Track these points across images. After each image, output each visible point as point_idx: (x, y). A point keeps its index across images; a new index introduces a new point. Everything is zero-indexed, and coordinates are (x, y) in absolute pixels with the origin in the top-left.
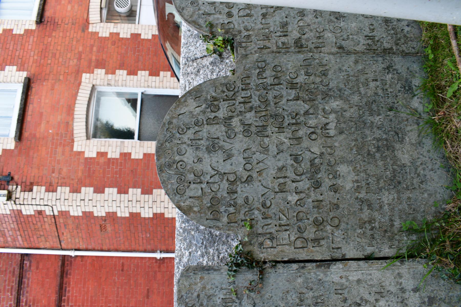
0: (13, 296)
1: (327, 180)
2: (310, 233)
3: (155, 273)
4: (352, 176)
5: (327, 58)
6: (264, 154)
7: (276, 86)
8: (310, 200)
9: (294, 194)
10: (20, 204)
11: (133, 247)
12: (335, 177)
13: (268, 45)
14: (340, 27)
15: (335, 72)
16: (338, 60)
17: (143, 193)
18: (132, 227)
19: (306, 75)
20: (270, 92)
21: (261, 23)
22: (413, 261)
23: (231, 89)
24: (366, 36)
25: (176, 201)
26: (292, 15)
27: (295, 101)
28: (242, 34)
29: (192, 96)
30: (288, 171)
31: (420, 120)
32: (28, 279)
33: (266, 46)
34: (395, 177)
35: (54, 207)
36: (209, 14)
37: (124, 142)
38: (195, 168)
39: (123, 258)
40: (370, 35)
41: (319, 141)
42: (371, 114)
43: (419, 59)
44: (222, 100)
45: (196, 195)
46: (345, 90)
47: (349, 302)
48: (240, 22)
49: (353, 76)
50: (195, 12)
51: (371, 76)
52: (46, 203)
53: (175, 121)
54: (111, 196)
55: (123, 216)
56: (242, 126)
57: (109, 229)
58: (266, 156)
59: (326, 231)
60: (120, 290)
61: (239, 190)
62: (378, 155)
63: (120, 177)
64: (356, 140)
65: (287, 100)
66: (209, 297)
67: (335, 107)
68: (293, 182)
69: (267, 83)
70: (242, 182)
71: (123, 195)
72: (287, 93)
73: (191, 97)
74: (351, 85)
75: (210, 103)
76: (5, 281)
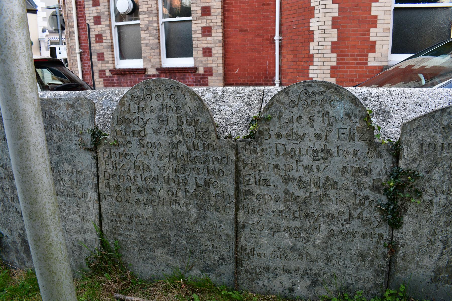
1: (143, 198)
2: (113, 183)
3: (261, 36)
4: (146, 215)
5: (230, 213)
6: (158, 157)
8: (130, 185)
9: (134, 175)
12: (144, 203)
13: (247, 168)
14: (263, 230)
15: (219, 217)
16: (229, 221)
17: (334, 18)
18: (301, 10)
19: (216, 194)
20: (202, 165)
21: (269, 163)
22: (99, 242)
25: (127, 95)
26: (277, 191)
28: (258, 146)
29: (199, 104)
30: (147, 173)
31: (183, 271)
33: (246, 165)
36: (280, 118)
38: (147, 107)
39: (275, 4)
41: (167, 197)
42: (187, 237)
45: (131, 109)
46: (204, 222)
47: (79, 200)
48: (271, 145)
50: (283, 104)
51: (216, 244)
53: (180, 91)
56: (176, 142)
58: (156, 158)
59: (114, 193)
61: (135, 138)
62: (159, 235)
64: (169, 223)
66: (78, 117)
68: (141, 175)
69: (209, 164)
70: (140, 140)
72: (202, 178)
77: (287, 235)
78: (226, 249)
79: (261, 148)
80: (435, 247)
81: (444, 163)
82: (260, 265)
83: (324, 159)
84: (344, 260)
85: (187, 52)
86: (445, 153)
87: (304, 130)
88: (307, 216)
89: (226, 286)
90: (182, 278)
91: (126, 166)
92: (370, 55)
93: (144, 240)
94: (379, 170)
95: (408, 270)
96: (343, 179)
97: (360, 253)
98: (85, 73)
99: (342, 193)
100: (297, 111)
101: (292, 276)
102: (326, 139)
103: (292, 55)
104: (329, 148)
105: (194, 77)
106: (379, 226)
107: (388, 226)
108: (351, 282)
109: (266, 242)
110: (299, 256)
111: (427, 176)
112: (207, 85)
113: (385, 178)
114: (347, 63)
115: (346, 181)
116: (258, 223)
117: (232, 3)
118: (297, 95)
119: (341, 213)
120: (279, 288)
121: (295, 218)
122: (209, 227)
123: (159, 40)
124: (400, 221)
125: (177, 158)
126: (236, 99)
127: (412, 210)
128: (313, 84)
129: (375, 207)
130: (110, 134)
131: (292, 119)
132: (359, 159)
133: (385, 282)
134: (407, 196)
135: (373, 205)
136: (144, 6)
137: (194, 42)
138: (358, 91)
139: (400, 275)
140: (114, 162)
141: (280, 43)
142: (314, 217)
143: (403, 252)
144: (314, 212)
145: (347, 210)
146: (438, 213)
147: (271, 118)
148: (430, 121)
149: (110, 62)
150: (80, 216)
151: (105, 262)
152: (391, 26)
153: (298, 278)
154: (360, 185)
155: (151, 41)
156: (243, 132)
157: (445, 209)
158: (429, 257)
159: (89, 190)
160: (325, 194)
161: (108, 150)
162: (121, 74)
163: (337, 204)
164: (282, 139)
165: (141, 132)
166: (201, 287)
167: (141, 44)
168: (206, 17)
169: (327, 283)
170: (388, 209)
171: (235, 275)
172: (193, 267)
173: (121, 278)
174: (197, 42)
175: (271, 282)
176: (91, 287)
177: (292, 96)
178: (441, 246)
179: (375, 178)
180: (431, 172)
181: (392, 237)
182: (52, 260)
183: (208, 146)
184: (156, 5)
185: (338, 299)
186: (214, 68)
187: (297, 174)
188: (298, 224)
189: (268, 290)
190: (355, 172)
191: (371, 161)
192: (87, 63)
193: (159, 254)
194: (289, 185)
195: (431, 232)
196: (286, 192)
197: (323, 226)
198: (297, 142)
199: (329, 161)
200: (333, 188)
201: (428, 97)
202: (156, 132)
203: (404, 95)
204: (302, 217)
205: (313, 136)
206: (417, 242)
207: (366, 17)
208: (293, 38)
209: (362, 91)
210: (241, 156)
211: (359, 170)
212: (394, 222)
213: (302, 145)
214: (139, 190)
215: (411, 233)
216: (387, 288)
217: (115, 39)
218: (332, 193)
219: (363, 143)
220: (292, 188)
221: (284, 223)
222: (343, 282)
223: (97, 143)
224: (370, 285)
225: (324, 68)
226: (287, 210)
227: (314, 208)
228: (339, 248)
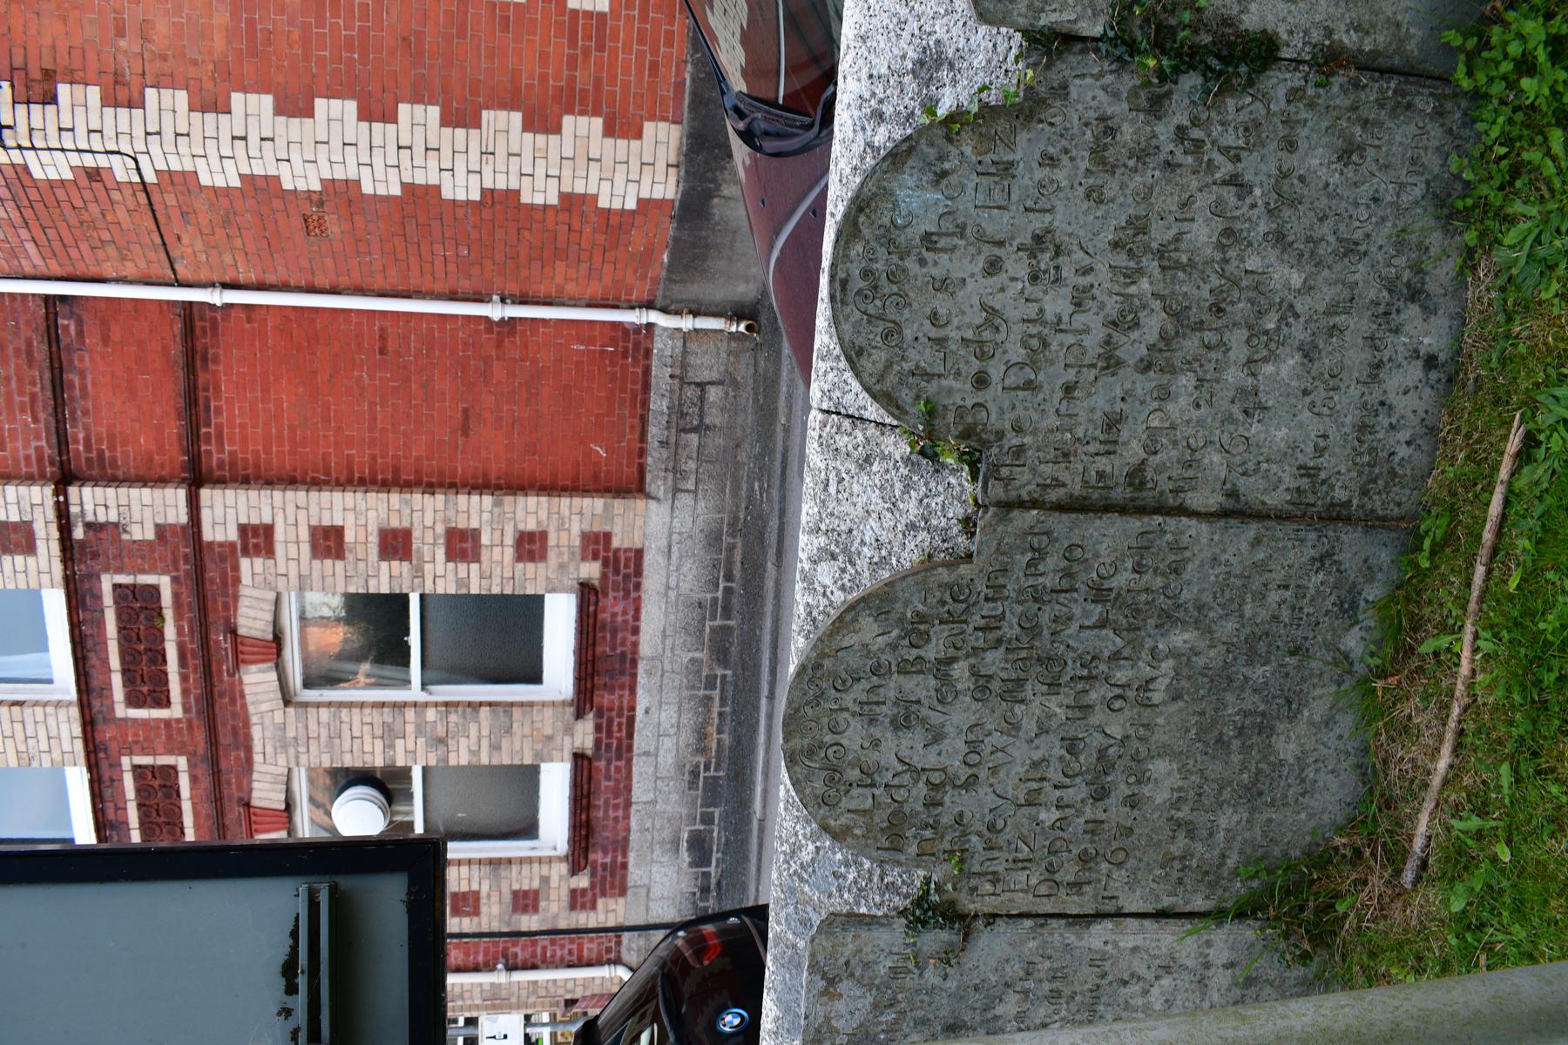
0: (42, 426)
1: (1123, 786)
3: (485, 363)
4: (1176, 781)
5: (1193, 532)
6: (1009, 735)
8: (1082, 820)
10: (20, 147)
12: (1139, 782)
13: (1064, 476)
15: (1201, 566)
16: (1216, 537)
17: (445, 122)
18: (411, 227)
19: (1134, 571)
20: (1047, 608)
26: (1139, 392)
28: (1005, 441)
32: (83, 375)
34: (1255, 784)
35: (143, 160)
36: (929, 376)
39: (384, 314)
41: (1127, 713)
42: (1250, 663)
45: (862, 807)
46: (1211, 609)
47: (1110, 978)
48: (1006, 405)
49: (1240, 576)
51: (1278, 576)
52: (112, 147)
53: (827, 663)
54: (336, 126)
55: (382, 191)
57: (334, 226)
61: (947, 799)
63: (364, 59)
64: (1202, 714)
66: (866, 965)
67: (1179, 644)
68: (1056, 787)
70: (955, 786)
71: (377, 126)
76: (8, 379)
77: (1269, 369)
79: (1010, 434)
82: (1349, 451)
83: (1057, 254)
85: (523, 615)
88: (1218, 310)
90: (1367, 680)
91: (1025, 832)
93: (1248, 789)
95: (1399, 17)
96: (1122, 199)
97: (1340, 158)
98: (575, 958)
101: (1390, 360)
102: (1001, 244)
103: (558, 263)
105: (611, 594)
106: (1266, 99)
108: (1423, 186)
109: (1284, 430)
112: (639, 553)
113: (1126, 77)
114: (598, 83)
117: (373, 458)
118: (869, 322)
119: (1218, 210)
121: (1221, 343)
122: (1227, 595)
123: (481, 704)
125: (1018, 679)
128: (841, 275)
130: (921, 873)
132: (1066, 152)
135: (1204, 117)
136: (368, 748)
137: (496, 590)
138: (851, 134)
139: (1413, 42)
140: (1010, 865)
141: (513, 303)
143: (1347, 31)
144: (1208, 287)
147: (927, 402)
149: (545, 871)
150: (1157, 978)
151: (1302, 909)
155: (485, 732)
156: (953, 480)
159: (1082, 943)
160: (1161, 253)
161: (973, 882)
162: (587, 837)
163: (1193, 220)
164: (992, 371)
165: (932, 780)
167: (490, 767)
168: (414, 547)
170: (1220, 73)
173: (1353, 864)
174: (496, 580)
176: (1372, 955)
179: (1126, 106)
181: (1300, 62)
182: (1364, 1030)
184: (367, 711)
186: (586, 527)
190: (1105, 164)
191: (1076, 118)
192: (544, 948)
193: (1292, 746)
196: (1145, 367)
197: (1253, 263)
198: (1003, 328)
200: (1144, 230)
202: (937, 737)
205: (991, 281)
207: (446, 12)
208: (499, 258)
209: (850, 122)
210: (1029, 493)
211: (1098, 154)
213: (1013, 314)
214: (1100, 794)
216: (1447, 81)
217: (471, 850)
218: (1159, 234)
219: (1023, 137)
220: (1133, 348)
221: (1234, 376)
222: (1419, 211)
223: (952, 916)
224: (1435, 132)
225: (608, 162)
228: (1321, 220)
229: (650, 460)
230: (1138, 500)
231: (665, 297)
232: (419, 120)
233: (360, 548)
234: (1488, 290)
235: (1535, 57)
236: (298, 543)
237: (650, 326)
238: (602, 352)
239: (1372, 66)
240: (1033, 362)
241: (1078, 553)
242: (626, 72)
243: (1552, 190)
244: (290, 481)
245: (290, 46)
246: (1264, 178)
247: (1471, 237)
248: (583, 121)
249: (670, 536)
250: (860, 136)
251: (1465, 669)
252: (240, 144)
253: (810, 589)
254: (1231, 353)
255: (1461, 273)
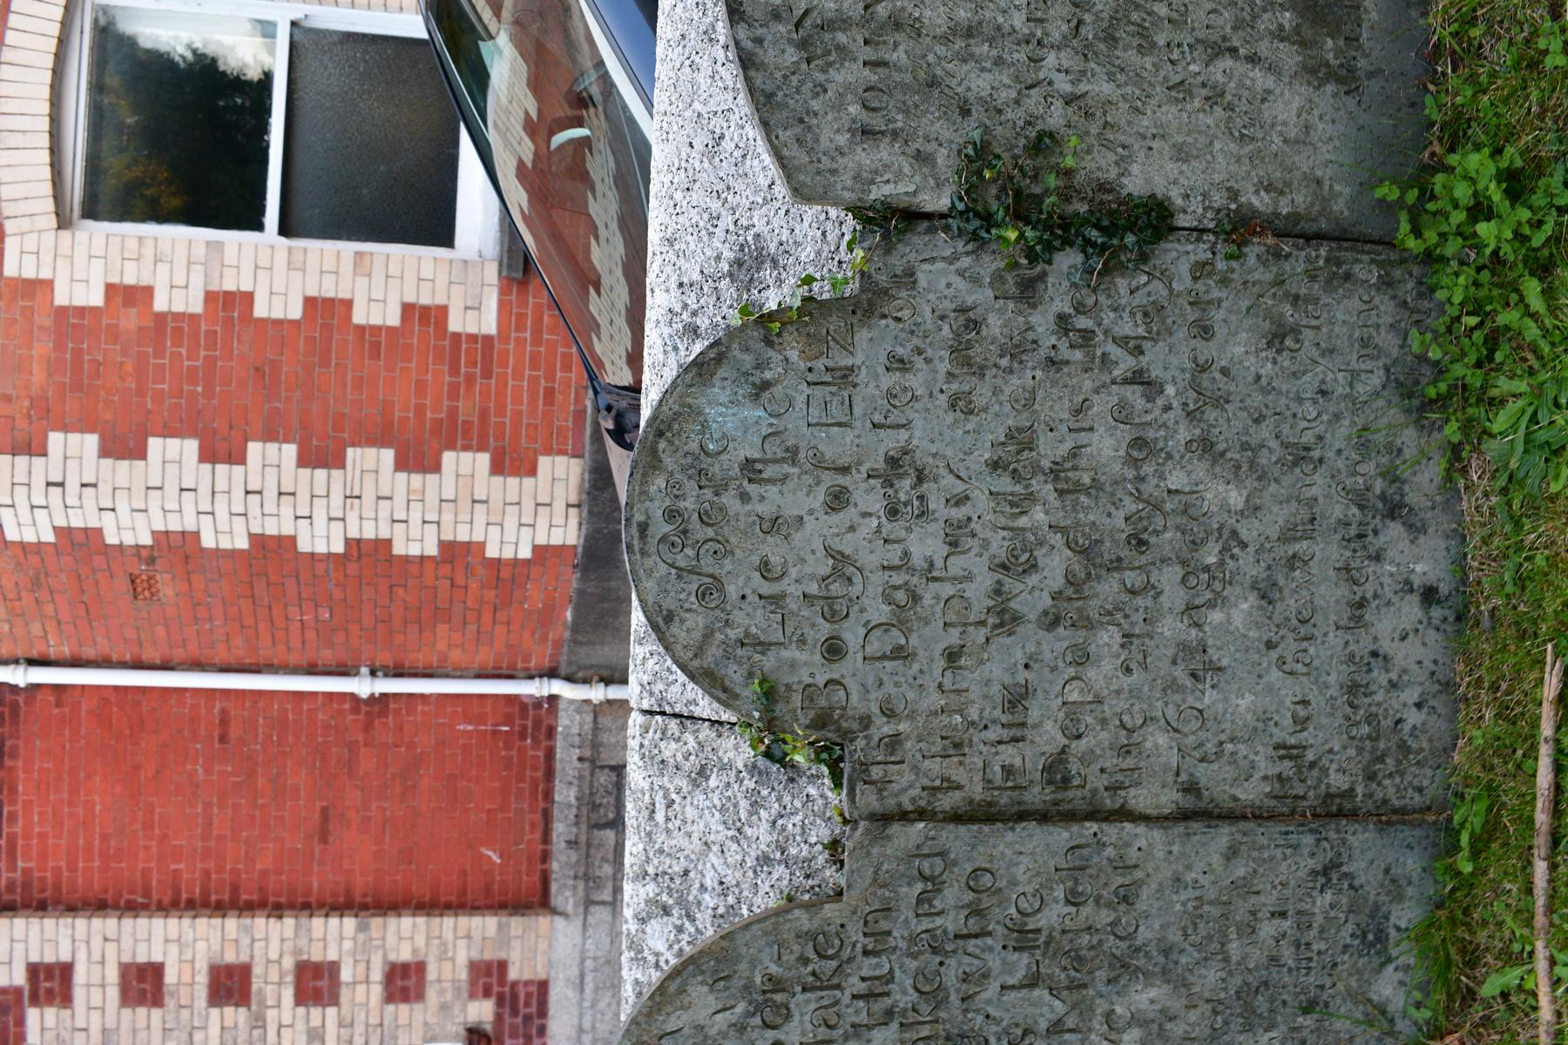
3: (350, 751)
5: (1142, 843)
7: (973, 941)
11: (261, 652)
13: (958, 775)
14: (1201, 712)
15: (1160, 890)
16: (1175, 849)
17: (304, 461)
18: (260, 588)
19: (1068, 902)
20: (951, 962)
21: (940, 686)
23: (830, 952)
24: (1277, 747)
26: (1047, 656)
27: (1024, 991)
28: (873, 730)
29: (703, 972)
33: (948, 780)
36: (763, 646)
37: (218, 246)
40: (1292, 741)
43: (1427, 837)
44: (799, 989)
46: (1182, 951)
48: (870, 680)
50: (713, 632)
51: (1269, 900)
54: (172, 470)
55: (225, 544)
57: (167, 588)
60: (215, 810)
63: (209, 392)
65: (1002, 987)
69: (945, 931)
71: (222, 469)
72: (1004, 961)
73: (700, 978)
74: (1204, 933)
75: (760, 998)
77: (1216, 616)
78: (1285, 859)
79: (879, 720)
80: (1232, 85)
81: (931, 58)
82: (1340, 721)
83: (920, 479)
84: (1300, 400)
86: (899, 56)
87: (813, 552)
89: (1437, 857)
92: (455, 324)
94: (958, 279)
95: (1319, 173)
96: (997, 407)
97: (1270, 344)
99: (1047, 411)
100: (740, 581)
101: (1375, 596)
102: (845, 470)
104: (881, 459)
106: (1166, 277)
107: (1164, 245)
108: (1382, 372)
109: (1249, 698)
110: (1293, 569)
111: (978, 113)
112: (543, 986)
113: (987, 258)
114: (484, 414)
115: (1004, 398)
116: (1176, 730)
117: (206, 873)
118: (679, 577)
119: (1122, 414)
120: (1425, 644)
121: (1149, 586)
122: (1203, 930)
124: (1146, 205)
126: (677, 823)
127: (1103, 163)
129: (1094, 291)
131: (771, 597)
132: (920, 352)
133: (1368, 253)
134: (1052, 181)
135: (1090, 301)
138: (661, 357)
139: (1341, 201)
141: (386, 675)
142: (1143, 514)
143: (1257, 192)
144: (1122, 514)
145: (1110, 394)
146: (1111, 77)
148: (782, 106)
152: (349, 248)
153: (1379, 571)
154: (1018, 346)
156: (812, 791)
157: (1095, 53)
158: (1267, 105)
160: (1055, 473)
163: (1091, 429)
164: (847, 636)
166: (1449, 962)
168: (254, 987)
169: (1392, 461)
170: (1103, 248)
171: (1388, 823)
172: (1370, 1000)
175: (1405, 678)
177: (683, 596)
178: (1227, 63)
179: (990, 293)
180: (965, 102)
181: (1203, 231)
183: (872, 935)
185: (1448, 420)
186: (475, 955)
187: (979, 579)
188: (1176, 572)
189: (1437, 687)
190: (970, 365)
191: (928, 310)
194: (1025, 610)
195: (1177, 99)
196: (1052, 621)
197: (1176, 480)
198: (857, 579)
199: (930, 460)
200: (1029, 445)
201: (688, 114)
203: (678, 196)
204: (1144, 559)
205: (835, 518)
206: (1217, 145)
208: (367, 620)
209: (659, 342)
210: (913, 800)
211: (960, 352)
212: (1150, 225)
213: (870, 560)
215: (1184, 167)
216: (1390, 245)
218: (1050, 449)
219: (862, 336)
220: (1032, 597)
221: (1171, 628)
224: (1386, 307)
225: (496, 503)
226: (1119, 616)
227: (1109, 515)
228: (1256, 421)
229: (555, 866)
230: (1061, 801)
231: (570, 663)
232: (271, 460)
233: (184, 991)
234: (1486, 495)
235: (1489, 198)
236: (103, 986)
237: (553, 699)
238: (495, 732)
239: (1295, 231)
240: (901, 624)
241: (987, 880)
242: (517, 400)
243: (1540, 357)
244: (99, 906)
245: (123, 380)
246: (1177, 373)
247: (1452, 431)
248: (466, 457)
249: (583, 961)
250: (672, 355)
251: (1546, 1013)
252: (55, 492)
253: (639, 960)
254: (1162, 599)
255: (1448, 478)
